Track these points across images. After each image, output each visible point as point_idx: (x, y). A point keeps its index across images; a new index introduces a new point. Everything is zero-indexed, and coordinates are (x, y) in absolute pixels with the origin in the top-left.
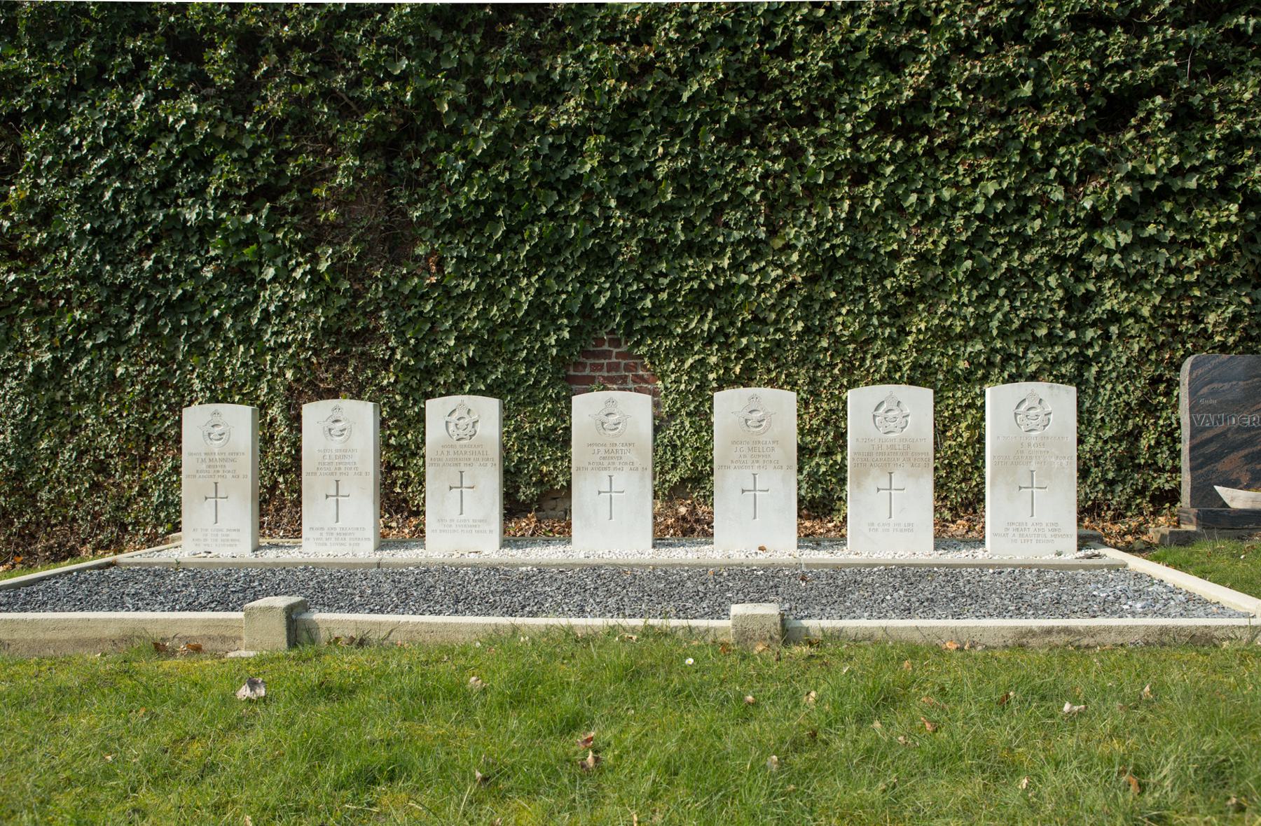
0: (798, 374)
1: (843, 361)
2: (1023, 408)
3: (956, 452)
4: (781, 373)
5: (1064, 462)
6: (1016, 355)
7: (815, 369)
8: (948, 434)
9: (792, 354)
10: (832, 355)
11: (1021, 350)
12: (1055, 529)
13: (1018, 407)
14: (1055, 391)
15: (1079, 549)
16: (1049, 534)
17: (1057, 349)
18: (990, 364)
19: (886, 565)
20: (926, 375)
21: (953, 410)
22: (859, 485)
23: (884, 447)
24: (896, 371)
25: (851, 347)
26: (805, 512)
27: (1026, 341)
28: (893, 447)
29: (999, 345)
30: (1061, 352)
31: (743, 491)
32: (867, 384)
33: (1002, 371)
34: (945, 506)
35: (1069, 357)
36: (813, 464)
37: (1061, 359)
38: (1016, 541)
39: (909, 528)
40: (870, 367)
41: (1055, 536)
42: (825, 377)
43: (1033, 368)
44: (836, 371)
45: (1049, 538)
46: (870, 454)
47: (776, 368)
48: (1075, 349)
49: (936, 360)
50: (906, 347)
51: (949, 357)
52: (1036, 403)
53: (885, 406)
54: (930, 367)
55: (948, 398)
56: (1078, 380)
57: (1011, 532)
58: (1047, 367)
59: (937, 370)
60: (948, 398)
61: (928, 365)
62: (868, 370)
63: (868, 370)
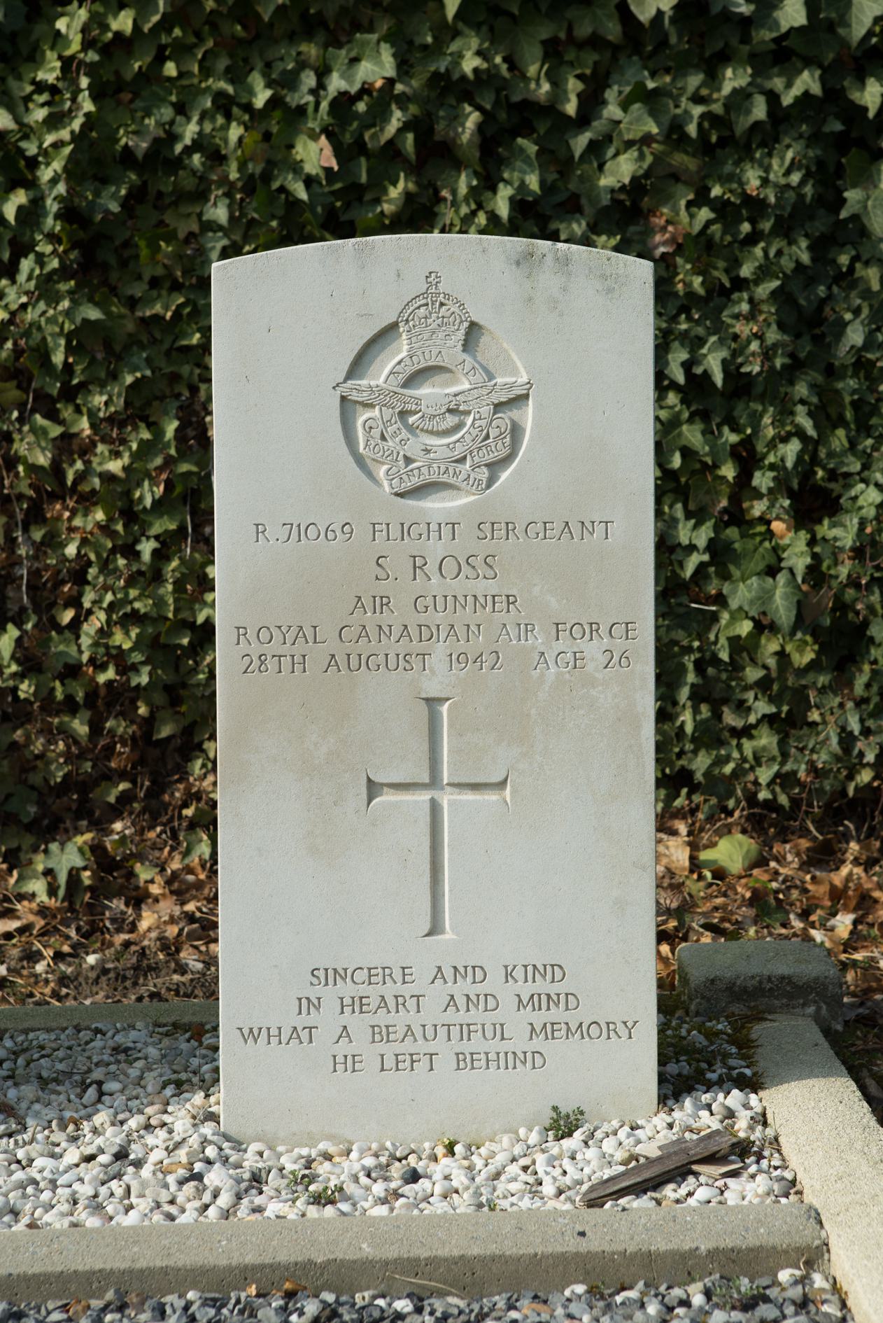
2: (382, 373)
5: (593, 650)
6: (551, 109)
11: (574, 86)
12: (549, 994)
14: (548, 280)
15: (673, 1088)
16: (517, 1023)
17: (733, 79)
18: (435, 153)
27: (595, 41)
29: (470, 64)
30: (740, 98)
31: (373, 789)
33: (489, 183)
35: (779, 115)
37: (742, 124)
38: (352, 1063)
41: (549, 1030)
43: (622, 169)
45: (519, 1041)
48: (808, 81)
49: (190, 130)
50: (50, 73)
51: (255, 117)
52: (449, 348)
54: (177, 164)
56: (820, 226)
57: (328, 1020)
58: (684, 161)
61: (161, 155)
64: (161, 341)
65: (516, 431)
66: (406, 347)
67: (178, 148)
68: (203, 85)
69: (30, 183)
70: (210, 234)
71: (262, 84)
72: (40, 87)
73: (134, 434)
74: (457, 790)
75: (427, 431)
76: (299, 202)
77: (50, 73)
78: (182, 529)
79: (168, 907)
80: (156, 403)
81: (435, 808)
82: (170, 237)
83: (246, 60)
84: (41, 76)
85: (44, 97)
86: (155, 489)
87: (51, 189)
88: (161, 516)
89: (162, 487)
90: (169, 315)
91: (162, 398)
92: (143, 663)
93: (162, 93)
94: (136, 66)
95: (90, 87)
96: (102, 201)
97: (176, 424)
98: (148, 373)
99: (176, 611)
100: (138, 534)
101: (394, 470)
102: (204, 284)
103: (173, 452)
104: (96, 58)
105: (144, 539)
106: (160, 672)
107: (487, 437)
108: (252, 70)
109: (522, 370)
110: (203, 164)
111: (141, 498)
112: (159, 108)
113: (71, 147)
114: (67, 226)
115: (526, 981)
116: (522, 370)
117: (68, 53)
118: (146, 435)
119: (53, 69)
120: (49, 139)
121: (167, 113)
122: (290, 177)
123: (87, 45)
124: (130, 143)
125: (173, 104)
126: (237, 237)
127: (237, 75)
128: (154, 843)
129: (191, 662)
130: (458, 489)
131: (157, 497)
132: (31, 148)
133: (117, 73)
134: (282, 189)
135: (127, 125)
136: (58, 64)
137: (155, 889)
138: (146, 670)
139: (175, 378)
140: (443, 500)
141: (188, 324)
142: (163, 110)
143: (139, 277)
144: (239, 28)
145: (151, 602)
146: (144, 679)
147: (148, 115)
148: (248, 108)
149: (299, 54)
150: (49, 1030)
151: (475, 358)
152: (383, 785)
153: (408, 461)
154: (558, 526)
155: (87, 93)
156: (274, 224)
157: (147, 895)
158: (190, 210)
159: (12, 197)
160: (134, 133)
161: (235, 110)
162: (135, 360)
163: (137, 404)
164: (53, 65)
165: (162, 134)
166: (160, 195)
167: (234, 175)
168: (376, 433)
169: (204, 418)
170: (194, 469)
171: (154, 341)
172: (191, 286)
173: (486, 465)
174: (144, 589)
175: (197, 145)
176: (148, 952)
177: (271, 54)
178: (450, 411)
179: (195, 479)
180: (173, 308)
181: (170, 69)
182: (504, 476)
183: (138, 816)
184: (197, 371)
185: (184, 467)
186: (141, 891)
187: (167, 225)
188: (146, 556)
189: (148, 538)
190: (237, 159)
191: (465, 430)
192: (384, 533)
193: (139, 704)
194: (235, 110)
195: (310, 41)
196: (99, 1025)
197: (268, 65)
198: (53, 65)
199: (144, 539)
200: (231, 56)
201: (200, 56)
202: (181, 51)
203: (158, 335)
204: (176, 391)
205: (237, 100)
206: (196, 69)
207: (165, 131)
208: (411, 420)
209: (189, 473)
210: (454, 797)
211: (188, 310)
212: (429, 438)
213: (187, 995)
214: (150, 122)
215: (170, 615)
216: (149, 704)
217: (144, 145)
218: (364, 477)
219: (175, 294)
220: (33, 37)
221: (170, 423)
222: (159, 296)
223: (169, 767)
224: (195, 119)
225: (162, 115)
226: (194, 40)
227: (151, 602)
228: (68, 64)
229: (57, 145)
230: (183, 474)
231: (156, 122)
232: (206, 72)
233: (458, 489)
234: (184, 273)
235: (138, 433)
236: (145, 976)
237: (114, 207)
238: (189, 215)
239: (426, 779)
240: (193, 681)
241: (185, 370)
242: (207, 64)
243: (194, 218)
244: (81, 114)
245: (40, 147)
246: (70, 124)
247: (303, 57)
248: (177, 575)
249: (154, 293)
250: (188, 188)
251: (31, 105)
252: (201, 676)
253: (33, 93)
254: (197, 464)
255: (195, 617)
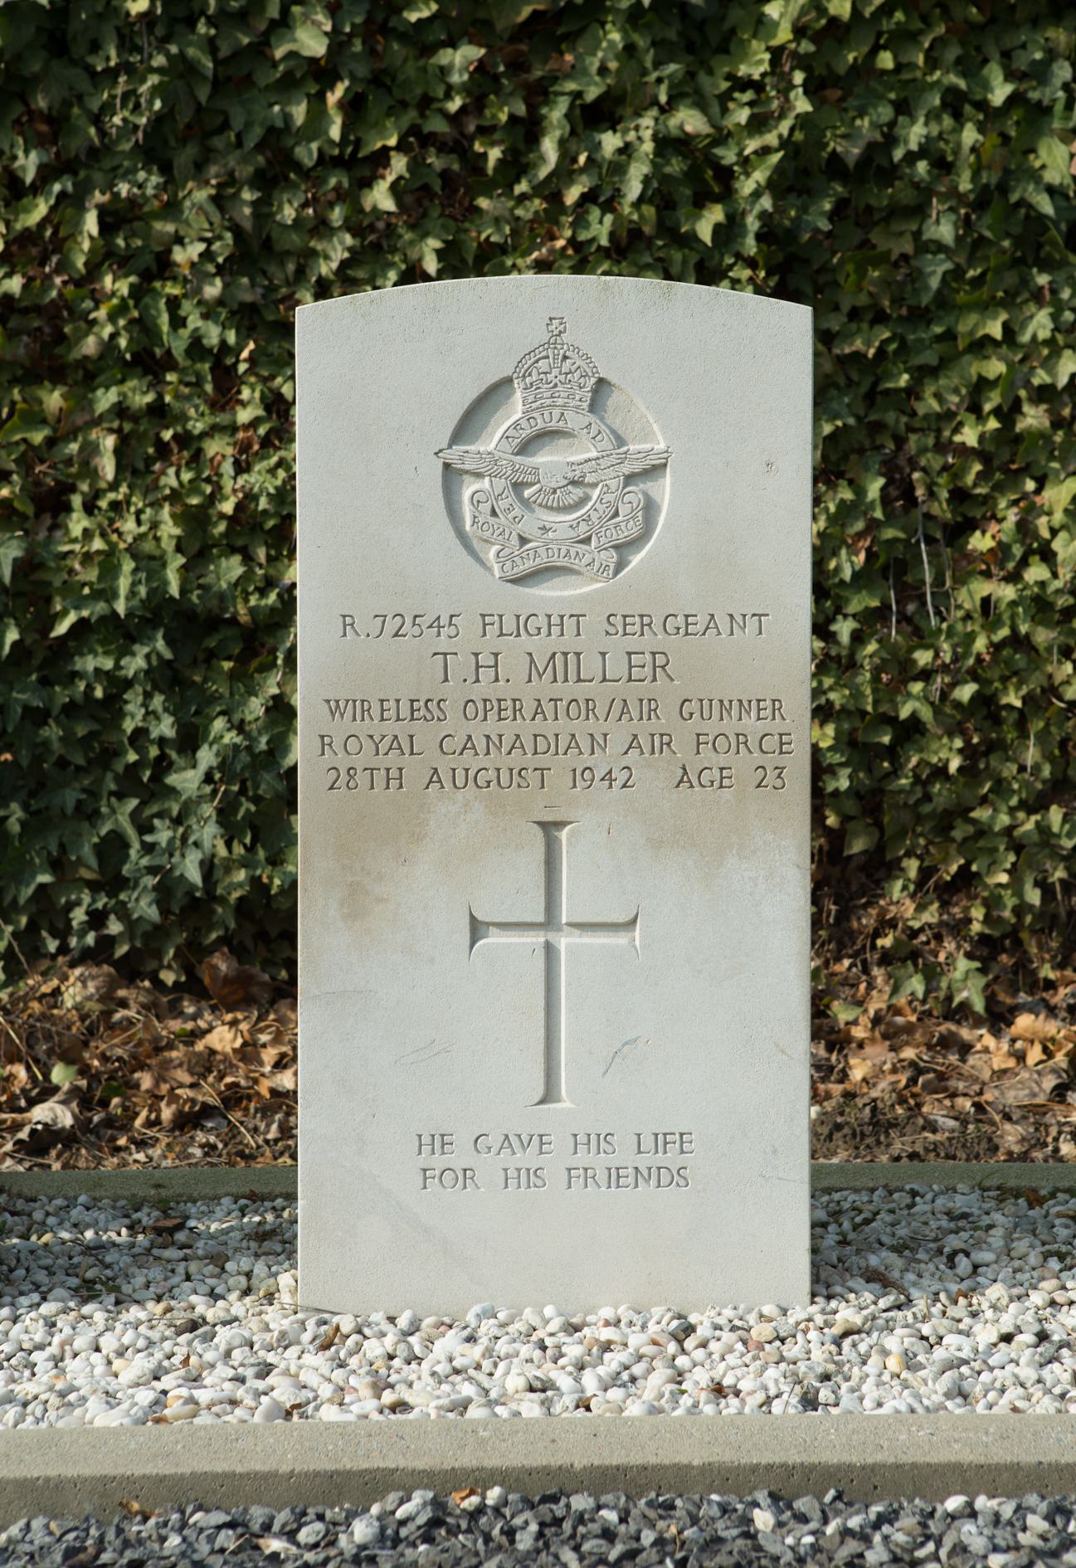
0: (172, 209)
1: (416, 141)
2: (493, 439)
3: (1018, 641)
4: (70, 203)
7: (270, 182)
8: (981, 542)
9: (134, 106)
10: (353, 107)
13: (467, 426)
19: (443, 1482)
20: (867, 218)
21: (1009, 413)
22: (356, 903)
23: (514, 665)
24: (700, 202)
25: (461, 58)
26: (222, 964)
28: (564, 665)
31: (476, 929)
32: (543, 267)
34: (958, 928)
36: (255, 708)
39: (663, 1159)
40: (566, 171)
42: (322, 228)
44: (380, 197)
46: (423, 709)
47: (46, 175)
49: (916, 133)
50: (756, 65)
51: (990, 117)
53: (515, 409)
54: (889, 173)
55: (982, 346)
59: (925, 192)
60: (982, 346)
61: (877, 164)
62: (551, 191)
63: (551, 191)
64: (858, 384)
65: (650, 508)
66: (520, 407)
67: (898, 154)
68: (929, 79)
69: (726, 194)
70: (930, 256)
71: (1001, 78)
72: (746, 84)
73: (831, 493)
74: (577, 932)
75: (546, 507)
76: (1042, 217)
77: (756, 65)
78: (886, 606)
79: (879, 1053)
80: (854, 457)
81: (550, 950)
82: (881, 259)
83: (978, 49)
84: (743, 70)
85: (748, 96)
86: (854, 558)
87: (753, 203)
88: (859, 591)
89: (862, 556)
90: (871, 352)
91: (861, 451)
92: (841, 765)
93: (880, 88)
94: (851, 57)
95: (805, 85)
96: (810, 218)
97: (881, 481)
98: (851, 421)
99: (876, 703)
100: (830, 612)
101: (507, 551)
102: (286, 330)
103: (878, 514)
104: (812, 48)
105: (840, 617)
106: (861, 775)
107: (616, 514)
108: (985, 61)
109: (660, 438)
110: (929, 172)
111: (838, 569)
112: (875, 107)
113: (781, 154)
114: (764, 247)
115: (653, 752)
116: (660, 438)
117: (775, 43)
118: (847, 494)
119: (761, 62)
120: (752, 146)
121: (885, 113)
122: (1031, 187)
123: (799, 31)
124: (839, 149)
125: (891, 102)
126: (961, 260)
127: (971, 66)
128: (846, 978)
129: (886, 764)
130: (578, 573)
131: (857, 568)
132: (728, 156)
133: (828, 67)
134: (1022, 202)
135: (835, 128)
136: (767, 56)
137: (859, 1033)
138: (845, 772)
139: (878, 427)
140: (548, 589)
141: (895, 364)
142: (880, 110)
143: (836, 308)
144: (974, 10)
145: (847, 692)
146: (844, 783)
147: (861, 116)
148: (982, 105)
149: (1047, 39)
150: (856, 1191)
151: (602, 419)
152: (488, 924)
153: (523, 541)
154: (702, 620)
155: (800, 90)
156: (1006, 243)
157: (848, 1039)
158: (903, 228)
159: (706, 213)
160: (843, 136)
161: (968, 109)
162: (835, 405)
163: (834, 458)
164: (759, 57)
165: (878, 137)
166: (869, 209)
167: (965, 185)
168: (485, 508)
169: (909, 475)
170: (901, 535)
171: (850, 383)
172: (900, 317)
173: (615, 547)
174: (839, 678)
175: (923, 152)
176: (880, 1105)
177: (1010, 41)
178: (573, 483)
179: (901, 547)
180: (877, 344)
181: (886, 60)
182: (636, 560)
183: (822, 945)
184: (904, 419)
185: (889, 533)
186: (842, 1035)
187: (874, 247)
188: (845, 637)
189: (845, 616)
190: (970, 166)
191: (590, 504)
192: (497, 626)
193: (827, 813)
194: (968, 109)
195: (1057, 26)
196: (916, 1187)
197: (1006, 55)
198: (759, 57)
199: (840, 617)
200: (963, 44)
201: (926, 45)
202: (901, 39)
203: (855, 377)
204: (878, 442)
205: (971, 97)
206: (920, 60)
207: (882, 133)
208: (527, 493)
209: (896, 540)
210: (570, 940)
211: (893, 347)
212: (550, 493)
213: (948, 1157)
214: (864, 123)
215: (869, 708)
216: (838, 813)
217: (856, 151)
218: (470, 560)
219: (878, 328)
220: (727, 26)
221: (872, 482)
222: (859, 330)
223: (854, 888)
224: (922, 120)
225: (879, 115)
226: (921, 25)
227: (847, 692)
228: (777, 53)
229: (765, 151)
230: (888, 541)
231: (871, 123)
232: (932, 63)
233: (578, 573)
234: (893, 302)
235: (835, 492)
236: (887, 1135)
237: (824, 225)
238: (901, 234)
239: (541, 919)
240: (893, 787)
241: (890, 417)
242: (935, 54)
243: (909, 237)
244: (793, 114)
245: (740, 154)
246: (776, 127)
247: (1050, 45)
248: (877, 660)
249: (853, 326)
250: (905, 202)
251: (731, 105)
252: (903, 781)
253: (731, 90)
254: (903, 529)
255: (897, 711)
